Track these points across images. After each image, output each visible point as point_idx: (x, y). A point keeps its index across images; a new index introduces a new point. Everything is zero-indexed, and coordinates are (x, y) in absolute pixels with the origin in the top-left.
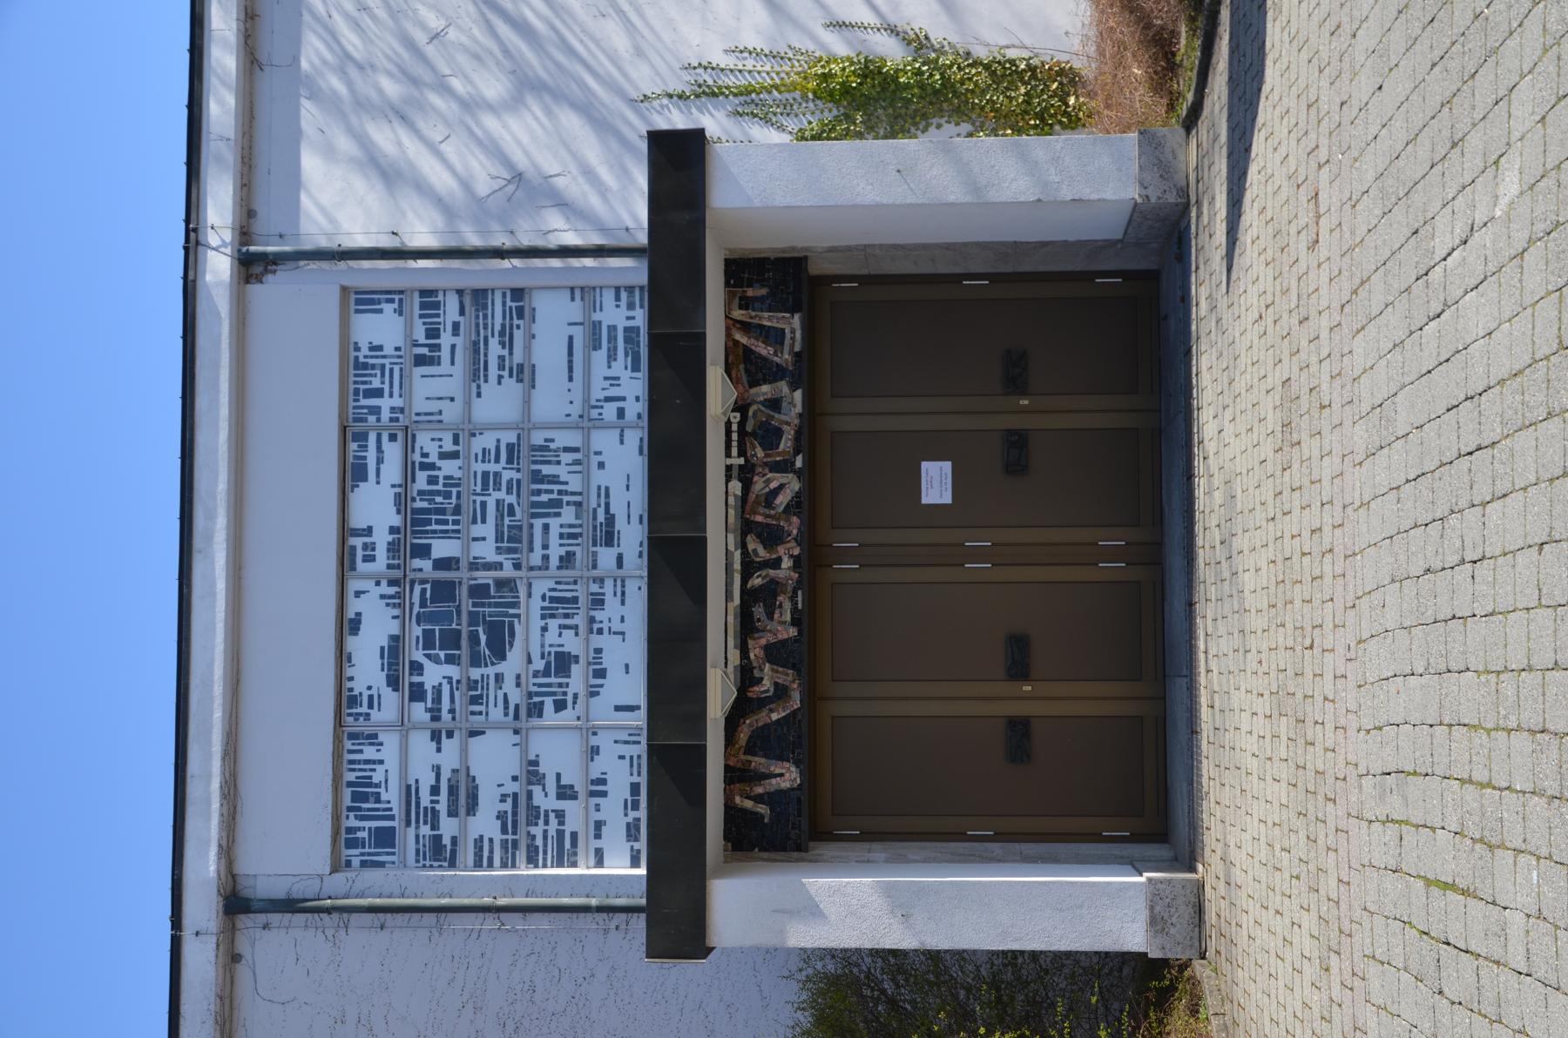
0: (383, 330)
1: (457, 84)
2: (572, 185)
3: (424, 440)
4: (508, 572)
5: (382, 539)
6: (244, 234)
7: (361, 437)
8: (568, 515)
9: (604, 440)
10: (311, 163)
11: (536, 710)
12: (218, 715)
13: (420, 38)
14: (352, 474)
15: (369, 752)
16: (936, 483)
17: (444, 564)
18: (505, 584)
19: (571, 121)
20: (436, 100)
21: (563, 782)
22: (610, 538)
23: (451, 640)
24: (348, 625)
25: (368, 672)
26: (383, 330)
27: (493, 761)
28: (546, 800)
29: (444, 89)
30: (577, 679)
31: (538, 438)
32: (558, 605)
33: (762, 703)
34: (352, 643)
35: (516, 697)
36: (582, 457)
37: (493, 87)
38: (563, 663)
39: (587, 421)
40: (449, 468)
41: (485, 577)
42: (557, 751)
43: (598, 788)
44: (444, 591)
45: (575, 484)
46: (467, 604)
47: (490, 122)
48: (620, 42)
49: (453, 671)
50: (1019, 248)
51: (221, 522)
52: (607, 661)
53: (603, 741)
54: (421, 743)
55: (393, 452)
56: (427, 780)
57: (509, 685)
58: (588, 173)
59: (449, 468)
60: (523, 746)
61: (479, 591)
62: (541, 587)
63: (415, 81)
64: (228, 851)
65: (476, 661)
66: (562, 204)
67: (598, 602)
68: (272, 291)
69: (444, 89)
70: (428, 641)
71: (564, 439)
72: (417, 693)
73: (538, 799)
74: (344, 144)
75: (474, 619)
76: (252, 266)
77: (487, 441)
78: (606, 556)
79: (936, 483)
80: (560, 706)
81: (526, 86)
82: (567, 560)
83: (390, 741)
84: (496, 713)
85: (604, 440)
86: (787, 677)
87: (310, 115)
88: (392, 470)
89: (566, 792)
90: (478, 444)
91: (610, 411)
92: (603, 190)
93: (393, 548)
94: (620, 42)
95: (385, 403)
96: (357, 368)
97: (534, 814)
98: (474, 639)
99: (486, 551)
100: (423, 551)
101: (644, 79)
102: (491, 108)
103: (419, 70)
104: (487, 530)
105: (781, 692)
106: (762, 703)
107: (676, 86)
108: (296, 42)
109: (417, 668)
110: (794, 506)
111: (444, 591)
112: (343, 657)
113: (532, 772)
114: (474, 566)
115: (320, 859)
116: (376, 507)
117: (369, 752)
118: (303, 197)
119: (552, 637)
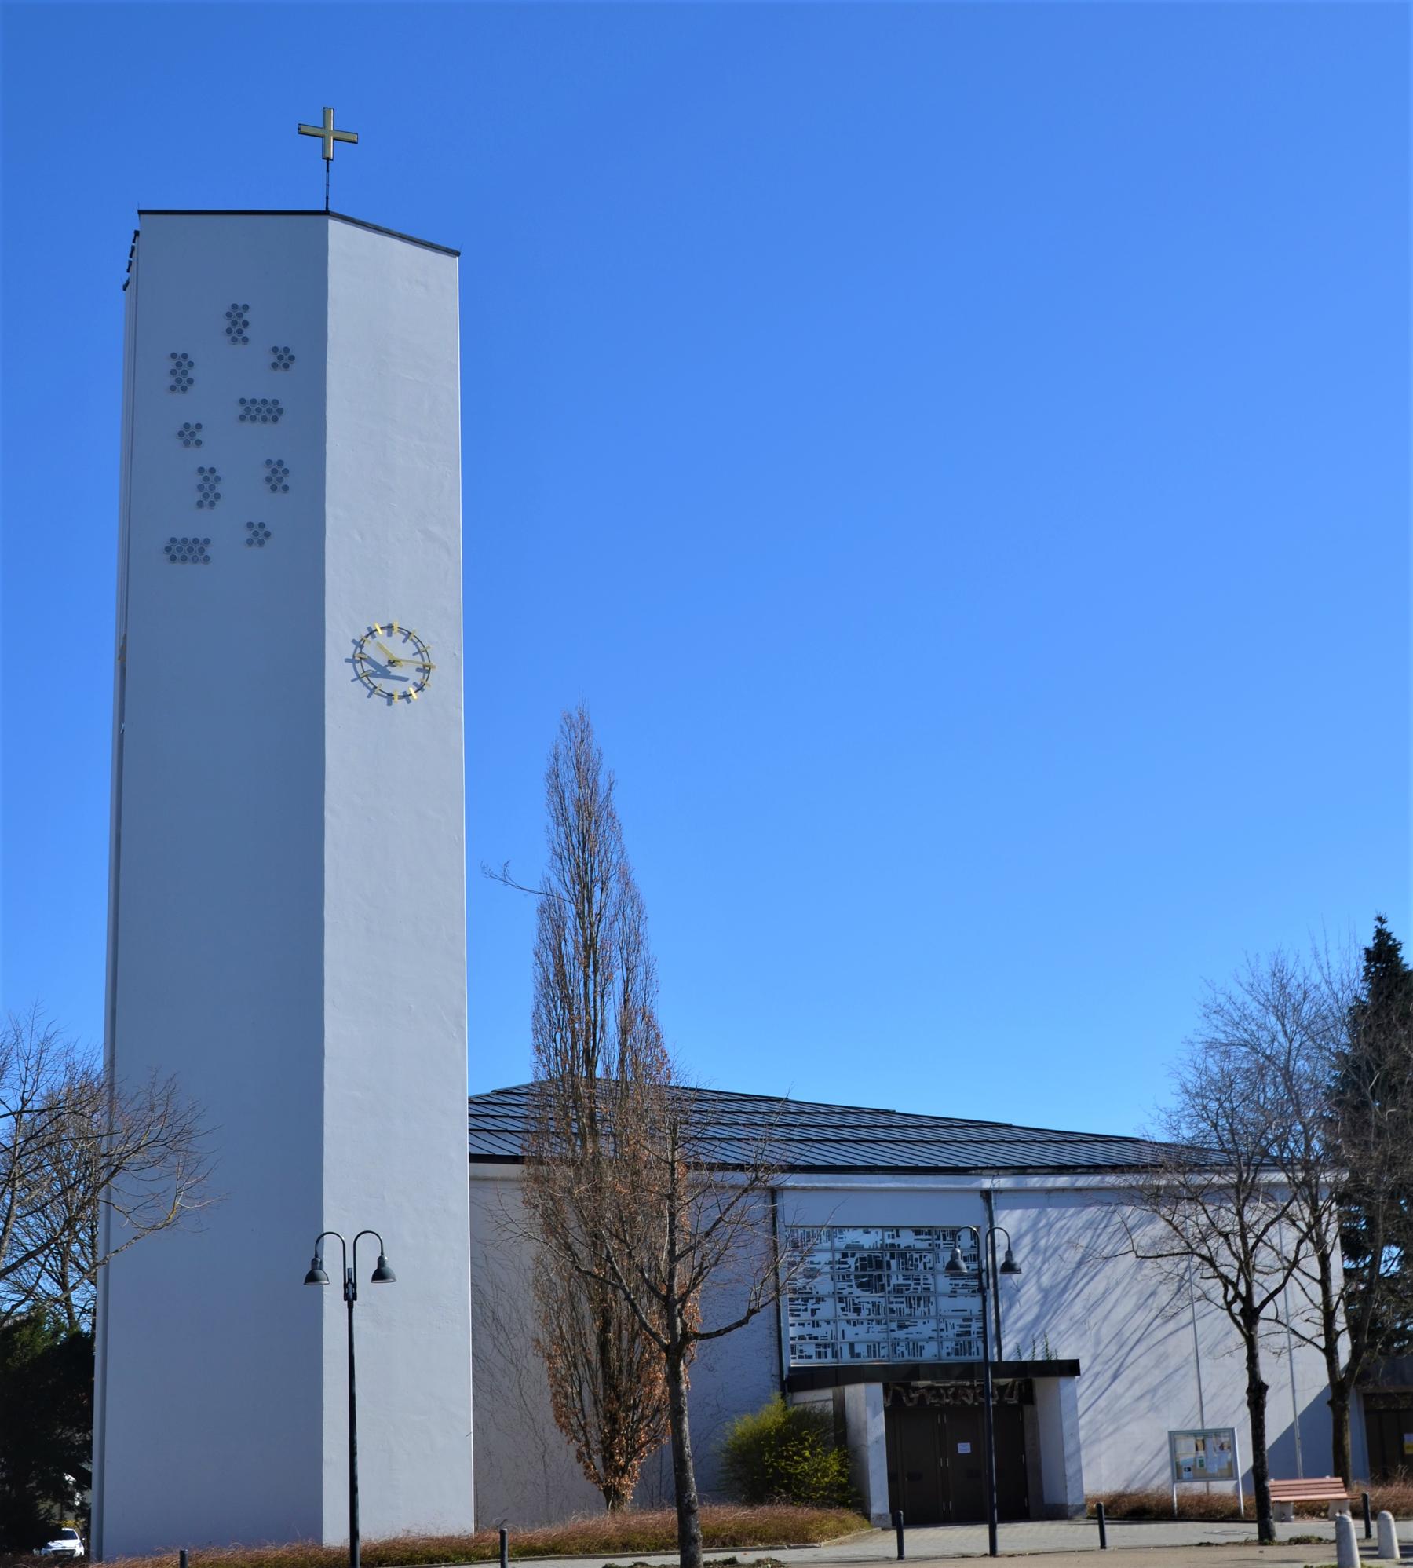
0: (966, 1241)
1: (1046, 1266)
2: (1016, 1310)
3: (929, 1257)
4: (888, 1289)
5: (896, 1241)
6: (999, 1191)
7: (929, 1233)
8: (907, 1311)
9: (933, 1324)
10: (1018, 1213)
11: (841, 1300)
12: (840, 1185)
13: (1060, 1252)
14: (917, 1231)
15: (824, 1238)
16: (964, 1448)
17: (888, 1263)
18: (883, 1289)
19: (1035, 1310)
20: (1040, 1260)
21: (1041, 1384)
22: (900, 1327)
23: (863, 1268)
24: (867, 1229)
25: (851, 1237)
26: (966, 1241)
27: (823, 1285)
28: (811, 1304)
29: (1044, 1262)
30: (852, 1316)
31: (932, 1299)
32: (876, 1308)
33: (908, 1395)
34: (860, 1231)
35: (845, 1292)
36: (926, 1316)
37: (1046, 1280)
38: (857, 1310)
39: (940, 1318)
40: (921, 1266)
41: (885, 1280)
42: (827, 1309)
43: (815, 1324)
44: (879, 1265)
45: (918, 1313)
46: (876, 1273)
47: (1034, 1280)
48: (1062, 1327)
49: (853, 1269)
50: (1038, 1471)
51: (904, 1185)
52: (859, 1326)
53: (832, 1326)
54: (827, 1257)
55: (925, 1245)
56: (815, 1259)
57: (849, 1290)
58: (1020, 1317)
59: (921, 1266)
60: (828, 1296)
61: (880, 1278)
62: (883, 1301)
63: (1046, 1250)
64: (794, 1188)
65: (856, 1277)
66: (1010, 1307)
67: (879, 1322)
68: (979, 1202)
69: (1044, 1262)
70: (862, 1259)
71: (932, 1308)
72: (845, 1256)
73: (811, 1302)
74: (1024, 1226)
75: (871, 1276)
76: (987, 1195)
77: (931, 1280)
78: (894, 1325)
79: (964, 1448)
80: (843, 1309)
81: (1046, 1293)
82: (892, 1311)
83: (829, 1244)
84: (839, 1285)
85: (933, 1324)
86: (915, 1402)
87: (1033, 1212)
88: (919, 1245)
89: (814, 1312)
90: (930, 1277)
91: (943, 1326)
92: (1016, 1322)
93: (893, 1245)
94: (1062, 1327)
95: (941, 1242)
96: (954, 1233)
97: (806, 1300)
98: (864, 1276)
99: (894, 1281)
100: (892, 1257)
101: (1051, 1336)
102: (1039, 1279)
103: (1049, 1253)
104: (901, 1281)
105: (911, 1400)
106: (908, 1395)
107: (1050, 1347)
108: (1055, 1206)
109: (853, 1255)
110: (964, 1402)
111: (879, 1265)
112: (856, 1228)
113: (819, 1300)
114: (889, 1276)
115: (789, 1222)
116: (907, 1239)
117: (824, 1238)
118: (1006, 1212)
119: (866, 1306)
